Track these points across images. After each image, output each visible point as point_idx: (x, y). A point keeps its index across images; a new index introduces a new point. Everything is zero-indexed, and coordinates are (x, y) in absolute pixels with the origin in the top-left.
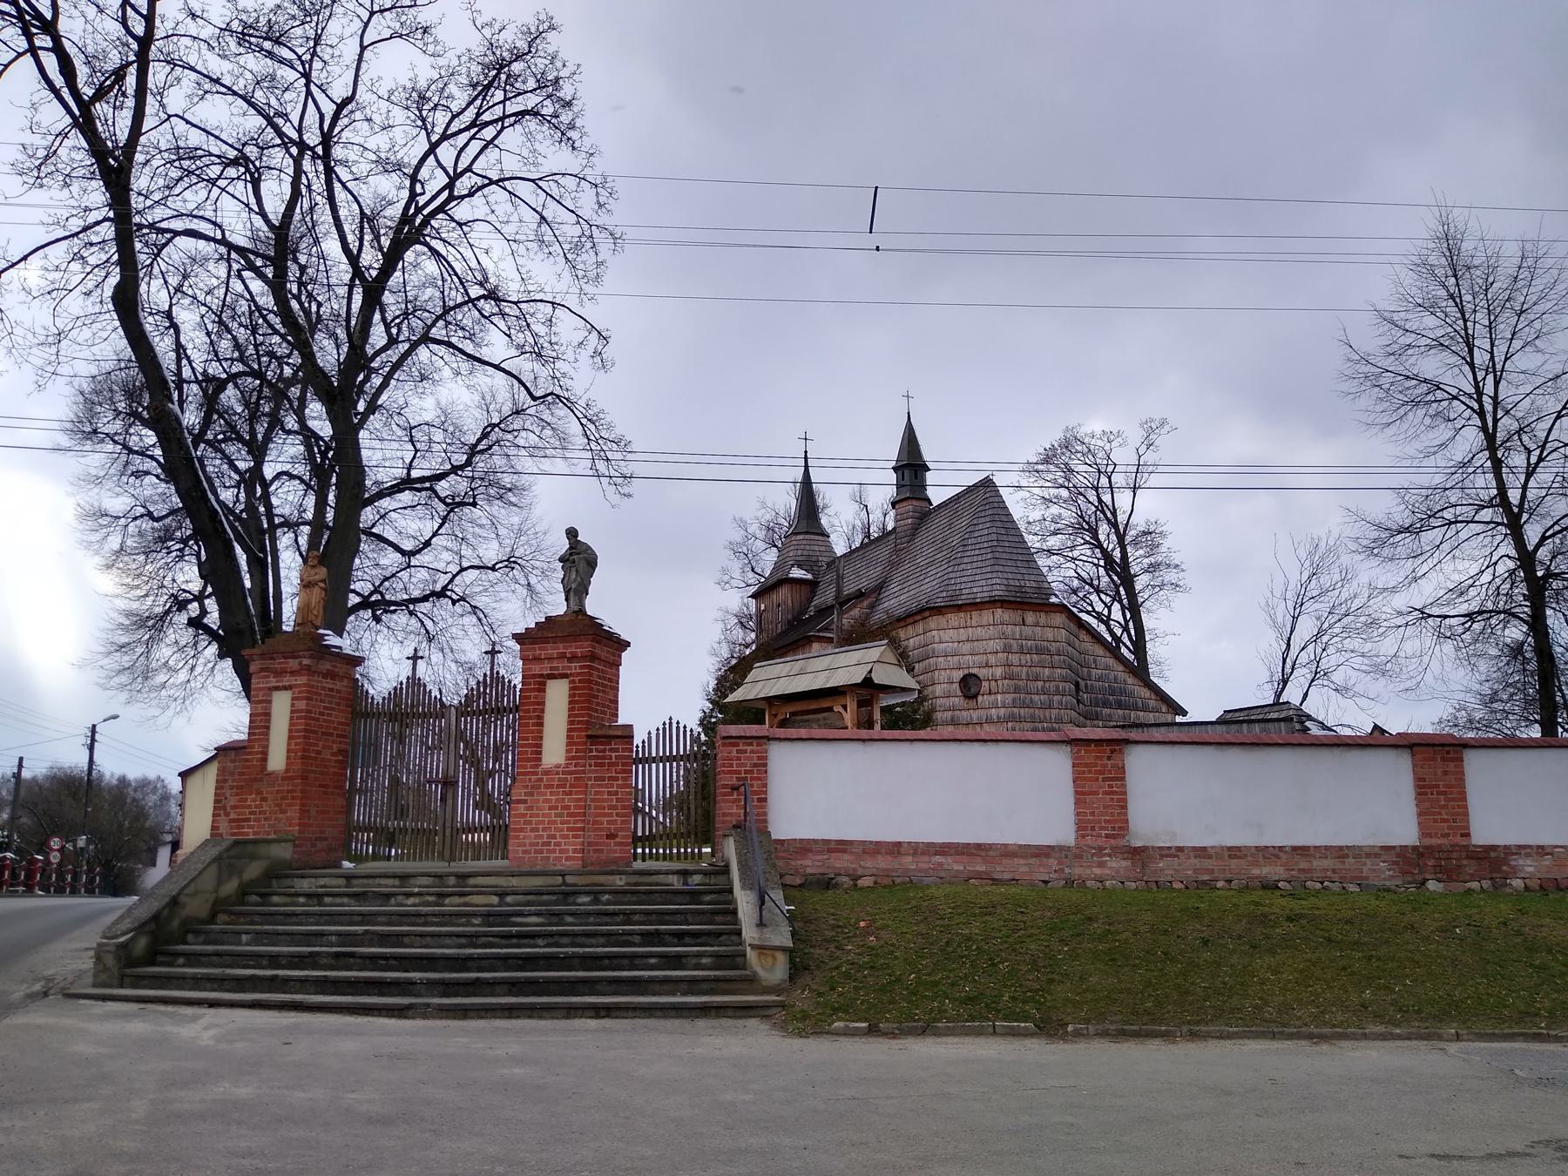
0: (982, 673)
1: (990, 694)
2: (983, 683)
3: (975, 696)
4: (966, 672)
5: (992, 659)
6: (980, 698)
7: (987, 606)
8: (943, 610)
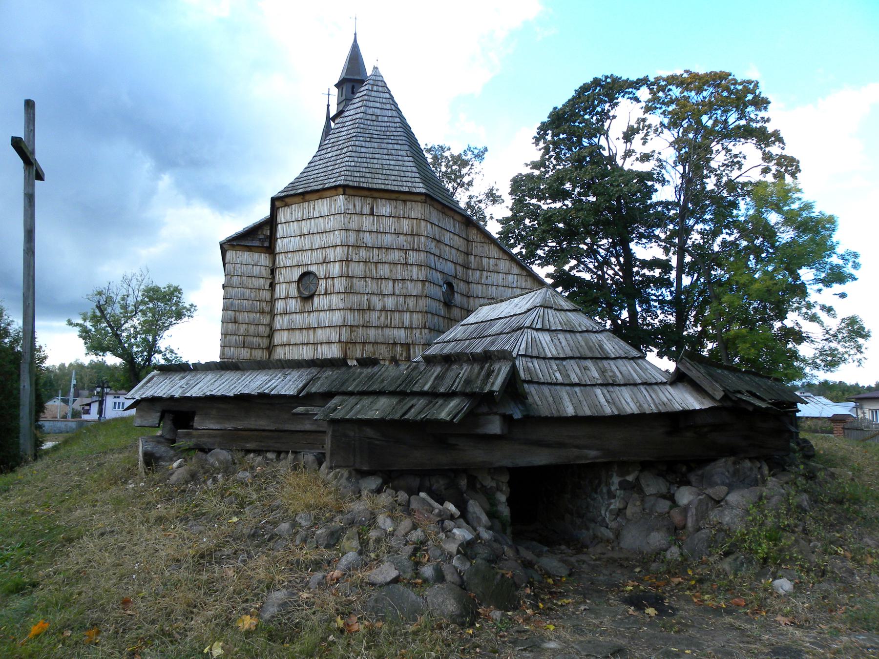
0: (320, 271)
1: (326, 294)
2: (321, 281)
3: (311, 297)
4: (305, 269)
5: (331, 254)
6: (316, 300)
7: (328, 193)
8: (287, 200)
